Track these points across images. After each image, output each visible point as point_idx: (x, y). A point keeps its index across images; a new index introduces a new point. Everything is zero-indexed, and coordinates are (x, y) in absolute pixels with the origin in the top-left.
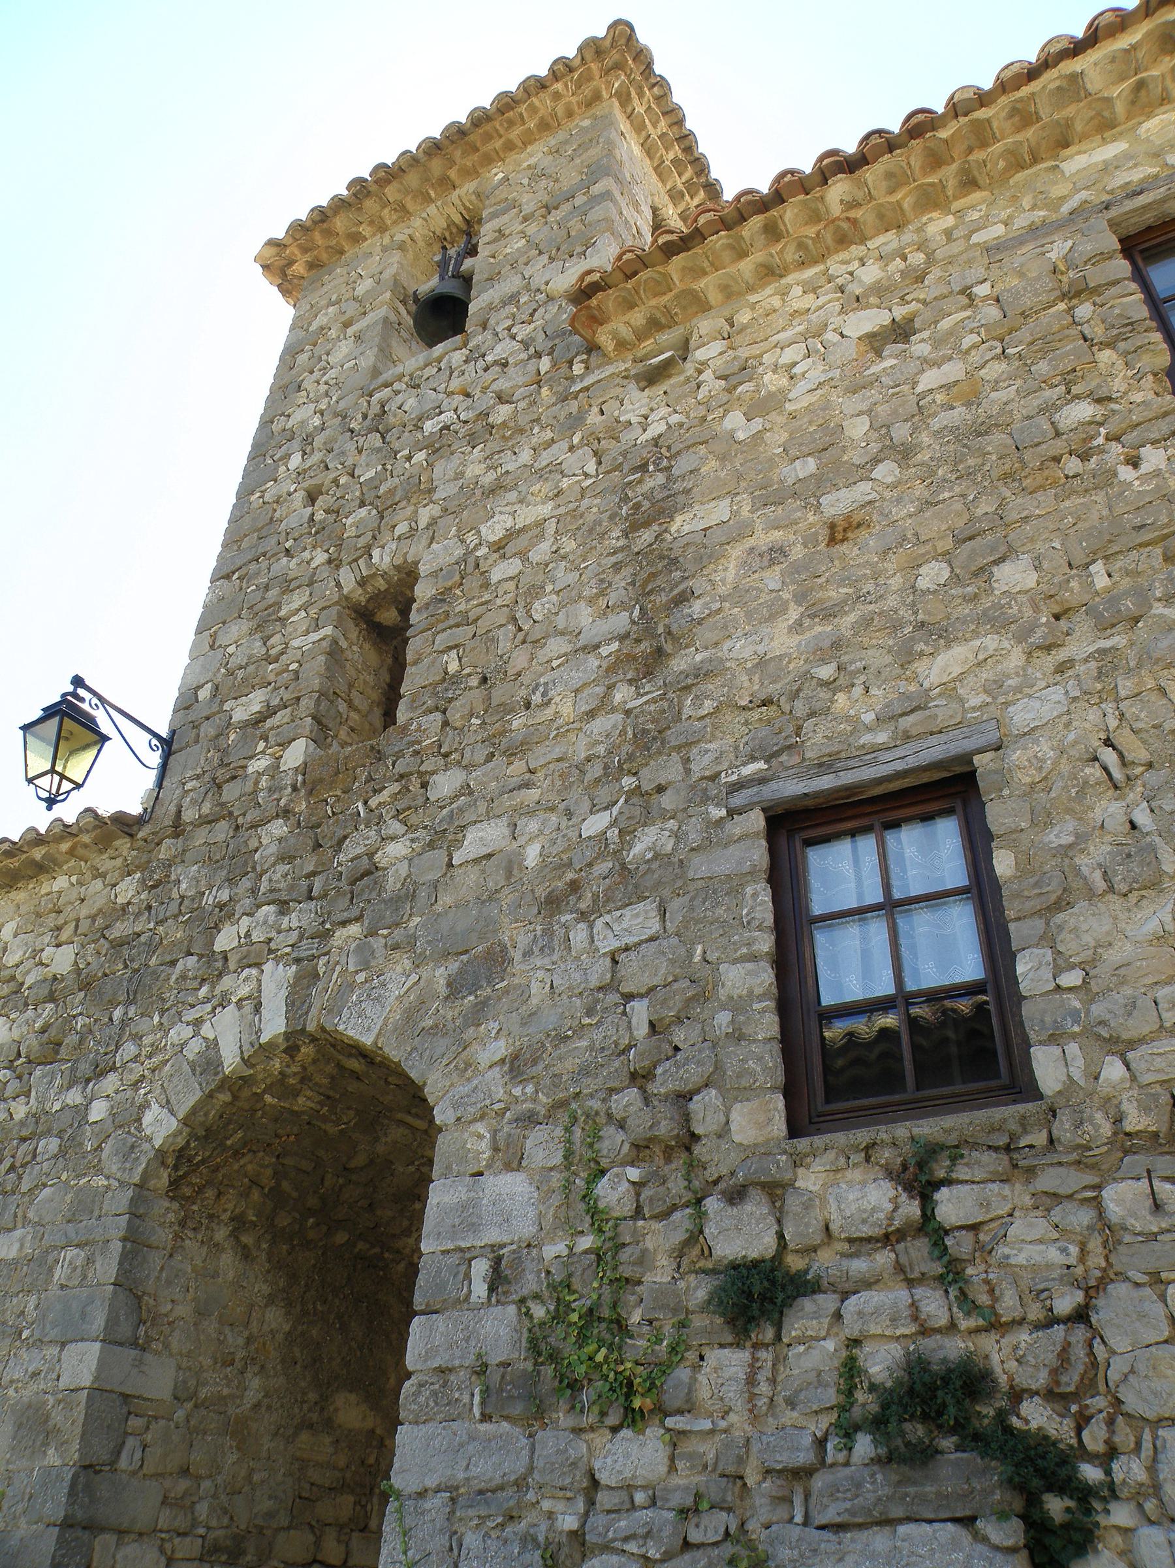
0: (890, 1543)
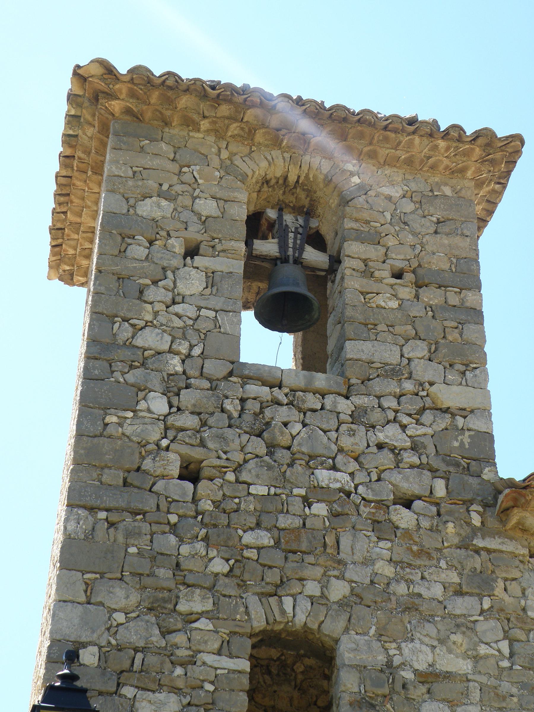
0: (312, 159)
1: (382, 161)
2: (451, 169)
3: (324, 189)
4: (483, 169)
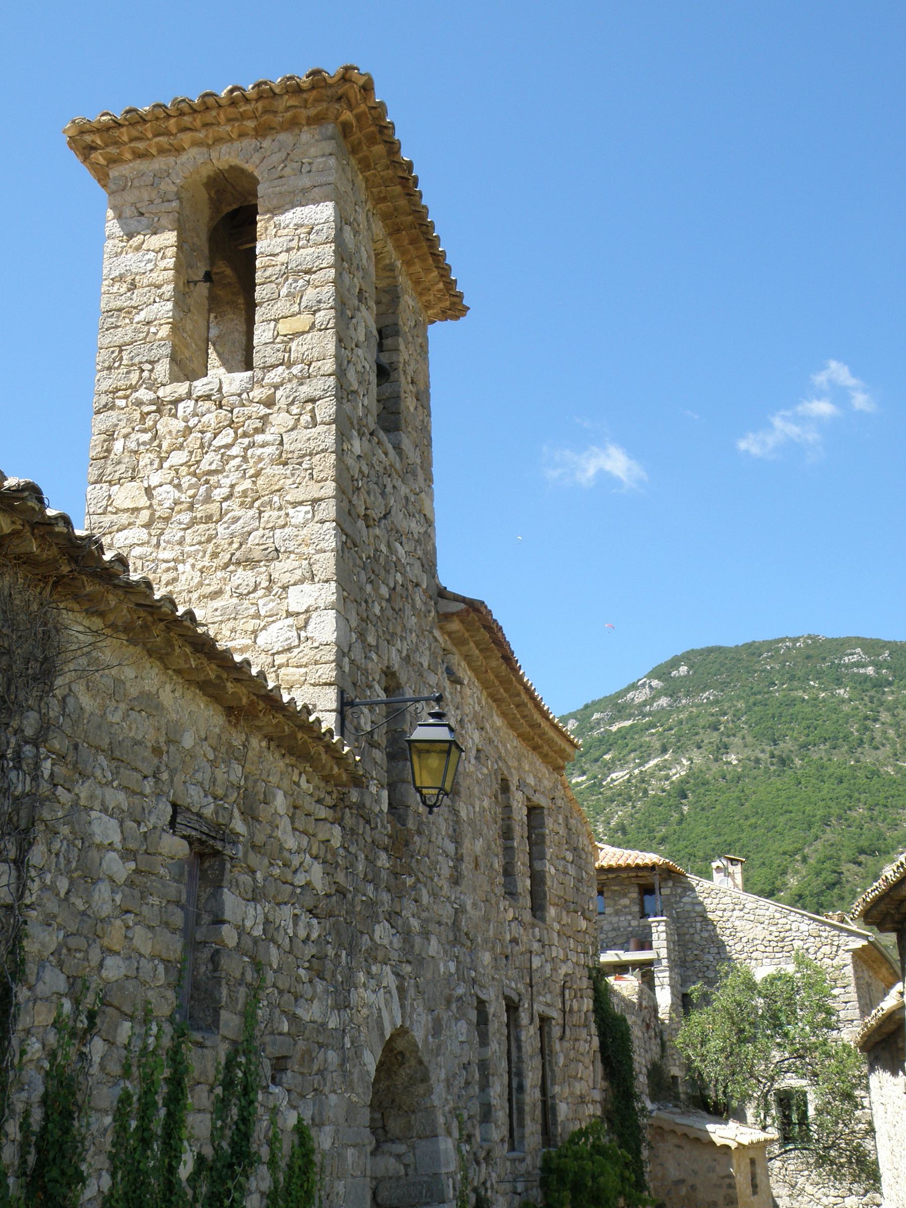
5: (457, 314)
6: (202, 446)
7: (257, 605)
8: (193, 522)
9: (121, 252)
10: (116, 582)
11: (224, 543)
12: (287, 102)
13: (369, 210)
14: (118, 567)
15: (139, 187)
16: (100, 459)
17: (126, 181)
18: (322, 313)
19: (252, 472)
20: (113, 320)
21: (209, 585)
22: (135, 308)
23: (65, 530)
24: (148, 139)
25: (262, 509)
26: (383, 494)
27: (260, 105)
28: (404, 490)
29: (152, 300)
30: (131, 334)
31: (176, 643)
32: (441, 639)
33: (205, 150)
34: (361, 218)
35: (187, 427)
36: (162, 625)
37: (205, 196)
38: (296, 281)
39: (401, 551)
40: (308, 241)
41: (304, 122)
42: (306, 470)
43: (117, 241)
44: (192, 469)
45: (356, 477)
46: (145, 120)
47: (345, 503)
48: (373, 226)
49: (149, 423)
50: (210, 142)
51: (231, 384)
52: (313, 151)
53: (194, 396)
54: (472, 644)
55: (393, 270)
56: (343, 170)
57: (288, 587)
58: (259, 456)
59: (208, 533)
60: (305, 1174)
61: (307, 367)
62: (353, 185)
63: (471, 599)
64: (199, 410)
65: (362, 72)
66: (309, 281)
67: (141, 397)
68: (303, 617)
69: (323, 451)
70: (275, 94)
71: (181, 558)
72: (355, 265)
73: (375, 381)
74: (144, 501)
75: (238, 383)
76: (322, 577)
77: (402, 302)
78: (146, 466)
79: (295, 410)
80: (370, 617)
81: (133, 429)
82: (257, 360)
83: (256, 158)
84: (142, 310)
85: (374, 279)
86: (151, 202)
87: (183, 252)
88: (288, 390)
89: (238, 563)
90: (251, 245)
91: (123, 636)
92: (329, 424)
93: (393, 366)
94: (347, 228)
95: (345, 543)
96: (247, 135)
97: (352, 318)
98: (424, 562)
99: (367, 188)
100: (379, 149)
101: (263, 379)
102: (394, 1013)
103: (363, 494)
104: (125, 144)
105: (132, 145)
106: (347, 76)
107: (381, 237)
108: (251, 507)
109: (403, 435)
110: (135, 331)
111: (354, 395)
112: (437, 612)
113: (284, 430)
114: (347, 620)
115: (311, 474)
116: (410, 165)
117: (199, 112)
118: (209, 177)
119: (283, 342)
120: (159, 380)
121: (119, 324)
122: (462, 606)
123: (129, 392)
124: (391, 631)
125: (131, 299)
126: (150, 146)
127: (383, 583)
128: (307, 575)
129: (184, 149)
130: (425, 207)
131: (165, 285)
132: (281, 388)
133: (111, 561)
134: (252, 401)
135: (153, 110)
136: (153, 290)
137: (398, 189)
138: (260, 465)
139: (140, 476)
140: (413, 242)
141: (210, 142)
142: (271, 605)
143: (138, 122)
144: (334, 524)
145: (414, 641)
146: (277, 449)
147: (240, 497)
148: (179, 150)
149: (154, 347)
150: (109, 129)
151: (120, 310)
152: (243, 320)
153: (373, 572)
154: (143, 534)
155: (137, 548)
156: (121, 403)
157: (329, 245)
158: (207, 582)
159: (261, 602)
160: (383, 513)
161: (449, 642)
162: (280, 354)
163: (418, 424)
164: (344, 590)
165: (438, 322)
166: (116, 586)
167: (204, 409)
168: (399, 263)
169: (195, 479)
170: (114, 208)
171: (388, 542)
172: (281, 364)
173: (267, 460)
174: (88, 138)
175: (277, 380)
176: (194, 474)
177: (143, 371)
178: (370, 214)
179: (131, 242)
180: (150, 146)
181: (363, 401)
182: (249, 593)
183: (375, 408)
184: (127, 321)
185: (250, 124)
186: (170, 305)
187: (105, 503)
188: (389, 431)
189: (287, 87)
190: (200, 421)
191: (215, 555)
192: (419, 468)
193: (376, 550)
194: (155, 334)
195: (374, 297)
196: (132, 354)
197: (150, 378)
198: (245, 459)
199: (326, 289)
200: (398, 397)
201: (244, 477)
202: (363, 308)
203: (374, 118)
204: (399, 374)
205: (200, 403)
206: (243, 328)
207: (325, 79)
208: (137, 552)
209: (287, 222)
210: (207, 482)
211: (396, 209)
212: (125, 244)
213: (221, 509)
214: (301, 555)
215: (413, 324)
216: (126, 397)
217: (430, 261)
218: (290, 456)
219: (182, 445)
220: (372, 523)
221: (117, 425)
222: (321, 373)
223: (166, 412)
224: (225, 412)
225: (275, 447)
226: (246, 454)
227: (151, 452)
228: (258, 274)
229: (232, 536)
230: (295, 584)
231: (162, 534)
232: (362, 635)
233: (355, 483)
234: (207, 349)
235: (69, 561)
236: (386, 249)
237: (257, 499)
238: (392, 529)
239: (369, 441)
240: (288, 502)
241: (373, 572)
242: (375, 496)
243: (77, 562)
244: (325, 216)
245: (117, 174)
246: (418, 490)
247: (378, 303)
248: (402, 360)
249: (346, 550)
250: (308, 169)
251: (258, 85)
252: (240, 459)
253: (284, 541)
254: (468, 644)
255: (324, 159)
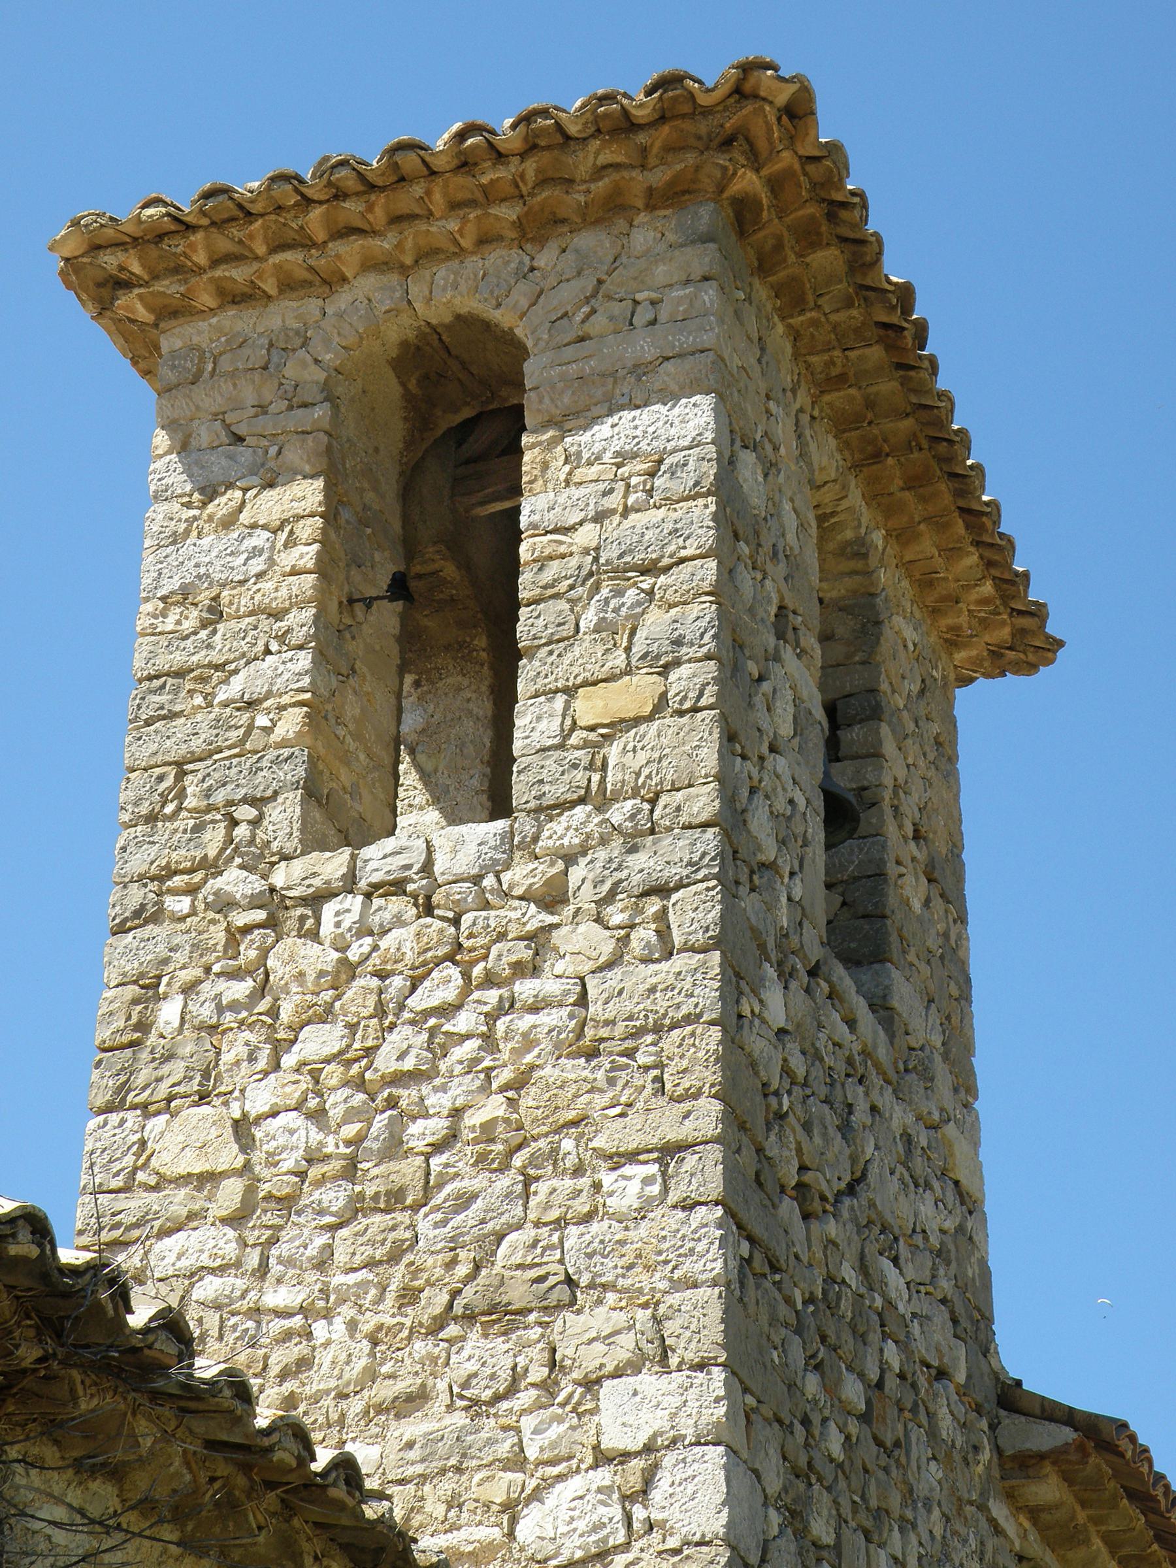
1: (907, 558)
2: (958, 636)
3: (830, 556)
4: (986, 664)
5: (1031, 657)
6: (380, 1011)
7: (518, 1431)
8: (356, 1208)
9: (187, 532)
10: (160, 1384)
11: (433, 1264)
12: (597, 154)
13: (801, 410)
14: (166, 1346)
15: (233, 374)
16: (123, 1047)
17: (202, 359)
18: (685, 670)
19: (505, 1076)
20: (163, 698)
21: (392, 1376)
22: (218, 667)
23: (34, 1251)
24: (257, 258)
25: (532, 1172)
26: (845, 1128)
27: (530, 167)
28: (899, 1117)
29: (260, 647)
30: (206, 733)
31: (306, 1546)
32: (1010, 1528)
33: (394, 278)
34: (783, 429)
35: (344, 962)
36: (271, 1499)
37: (394, 389)
38: (619, 593)
39: (895, 1280)
40: (650, 493)
41: (640, 204)
42: (647, 1068)
43: (176, 506)
44: (355, 1069)
45: (775, 1085)
46: (249, 214)
47: (748, 1156)
48: (813, 447)
49: (248, 953)
50: (408, 260)
51: (455, 852)
52: (661, 272)
53: (363, 884)
54: (1097, 1543)
55: (865, 556)
56: (737, 314)
57: (598, 1381)
58: (525, 1035)
59: (392, 1236)
60: (424, 1134)
61: (646, 806)
62: (762, 349)
63: (1090, 1415)
64: (375, 920)
65: (785, 72)
66: (650, 593)
67: (229, 888)
68: (637, 1464)
69: (688, 1019)
70: (568, 138)
71: (321, 1304)
72: (767, 548)
73: (821, 836)
74: (229, 1156)
75: (472, 848)
76: (689, 1355)
77: (887, 633)
78: (237, 1063)
79: (617, 917)
80: (818, 1465)
81: (208, 970)
82: (521, 791)
83: (521, 295)
84: (236, 672)
85: (815, 579)
86: (262, 409)
87: (337, 529)
88: (599, 864)
89: (469, 1317)
90: (507, 505)
91: (169, 1533)
92: (704, 950)
93: (867, 797)
94: (747, 458)
95: (749, 1261)
96: (500, 238)
97: (761, 679)
98: (960, 1309)
99: (796, 356)
100: (828, 258)
101: (536, 839)
102: (473, 501)
103: (794, 1131)
104: (200, 270)
105: (218, 273)
106: (748, 87)
107: (833, 475)
108: (502, 1170)
109: (895, 974)
110: (217, 723)
111: (768, 874)
112: (998, 1450)
113: (590, 965)
114: (755, 1472)
115: (659, 1080)
116: (906, 294)
117: (383, 189)
118: (404, 344)
119: (586, 744)
120: (275, 846)
121: (177, 708)
122: (1068, 1434)
123: (198, 877)
124: (874, 1503)
125: (209, 646)
126: (260, 274)
127: (850, 1368)
128: (649, 1349)
129: (344, 279)
130: (944, 396)
131: (294, 611)
132: (583, 861)
133: (146, 1331)
134: (507, 895)
135: (269, 188)
136: (265, 623)
137: (876, 353)
138: (529, 1058)
139: (222, 1089)
140: (913, 483)
141: (408, 260)
142: (556, 1430)
143: (233, 219)
144: (719, 1212)
145: (938, 1532)
146: (571, 1016)
147: (476, 1142)
148: (332, 282)
149: (265, 763)
150: (161, 237)
151: (180, 674)
152: (484, 688)
153: (823, 1339)
154: (225, 1242)
155: (209, 1278)
156: (182, 904)
157: (701, 501)
158: (386, 1369)
159: (528, 1423)
160: (847, 1178)
161: (1033, 1536)
162: (580, 776)
163: (933, 943)
164: (746, 1390)
165: (981, 683)
166: (156, 1396)
167: (387, 916)
168: (878, 538)
169: (361, 1097)
170: (170, 426)
171: (862, 1257)
172: (582, 801)
173: (546, 1045)
174: (110, 261)
175: (572, 840)
176: (360, 1084)
177: (235, 823)
178: (805, 419)
179: (211, 508)
180: (260, 274)
181: (788, 887)
182: (498, 1398)
183: (820, 906)
184: (198, 700)
185: (508, 213)
186: (304, 660)
187: (129, 1160)
188: (858, 963)
189: (597, 118)
190: (375, 948)
191: (409, 1296)
192: (938, 1058)
193: (830, 1279)
194: (268, 730)
195: (816, 624)
196: (209, 782)
197: (252, 842)
198: (489, 1041)
199: (694, 610)
200: (881, 875)
201: (485, 1089)
202: (788, 654)
203: (814, 185)
204: (881, 812)
205: (377, 902)
206: (484, 707)
207: (691, 96)
208: (208, 1288)
209: (597, 448)
210: (392, 1103)
211: (870, 404)
212: (196, 512)
213: (428, 1174)
214: (632, 1295)
215: (915, 688)
216: (191, 890)
217: (960, 528)
218: (604, 1032)
219: (329, 1009)
220: (817, 1205)
221: (166, 961)
222: (684, 819)
223: (291, 924)
224: (438, 924)
225: (564, 1012)
226: (491, 1028)
227: (250, 1027)
228: (525, 578)
229: (454, 1244)
230: (617, 1374)
231: (273, 1241)
232: (796, 1517)
233: (773, 1101)
234: (397, 762)
235: (39, 1333)
236: (845, 504)
237: (520, 1147)
238: (870, 1222)
239: (808, 991)
240: (599, 1153)
241: (823, 1339)
242: (824, 1135)
243: (59, 1335)
244: (691, 428)
245: (178, 344)
246: (936, 1116)
247: (826, 638)
248: (888, 781)
249: (751, 1281)
250: (650, 316)
251: (526, 119)
252: (472, 1045)
253: (590, 1256)
254: (1087, 1542)
255: (689, 290)
